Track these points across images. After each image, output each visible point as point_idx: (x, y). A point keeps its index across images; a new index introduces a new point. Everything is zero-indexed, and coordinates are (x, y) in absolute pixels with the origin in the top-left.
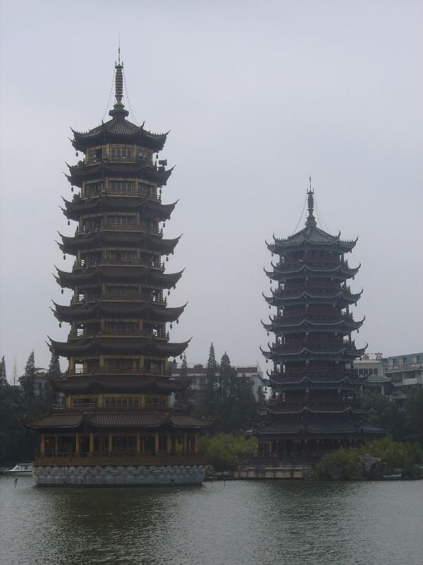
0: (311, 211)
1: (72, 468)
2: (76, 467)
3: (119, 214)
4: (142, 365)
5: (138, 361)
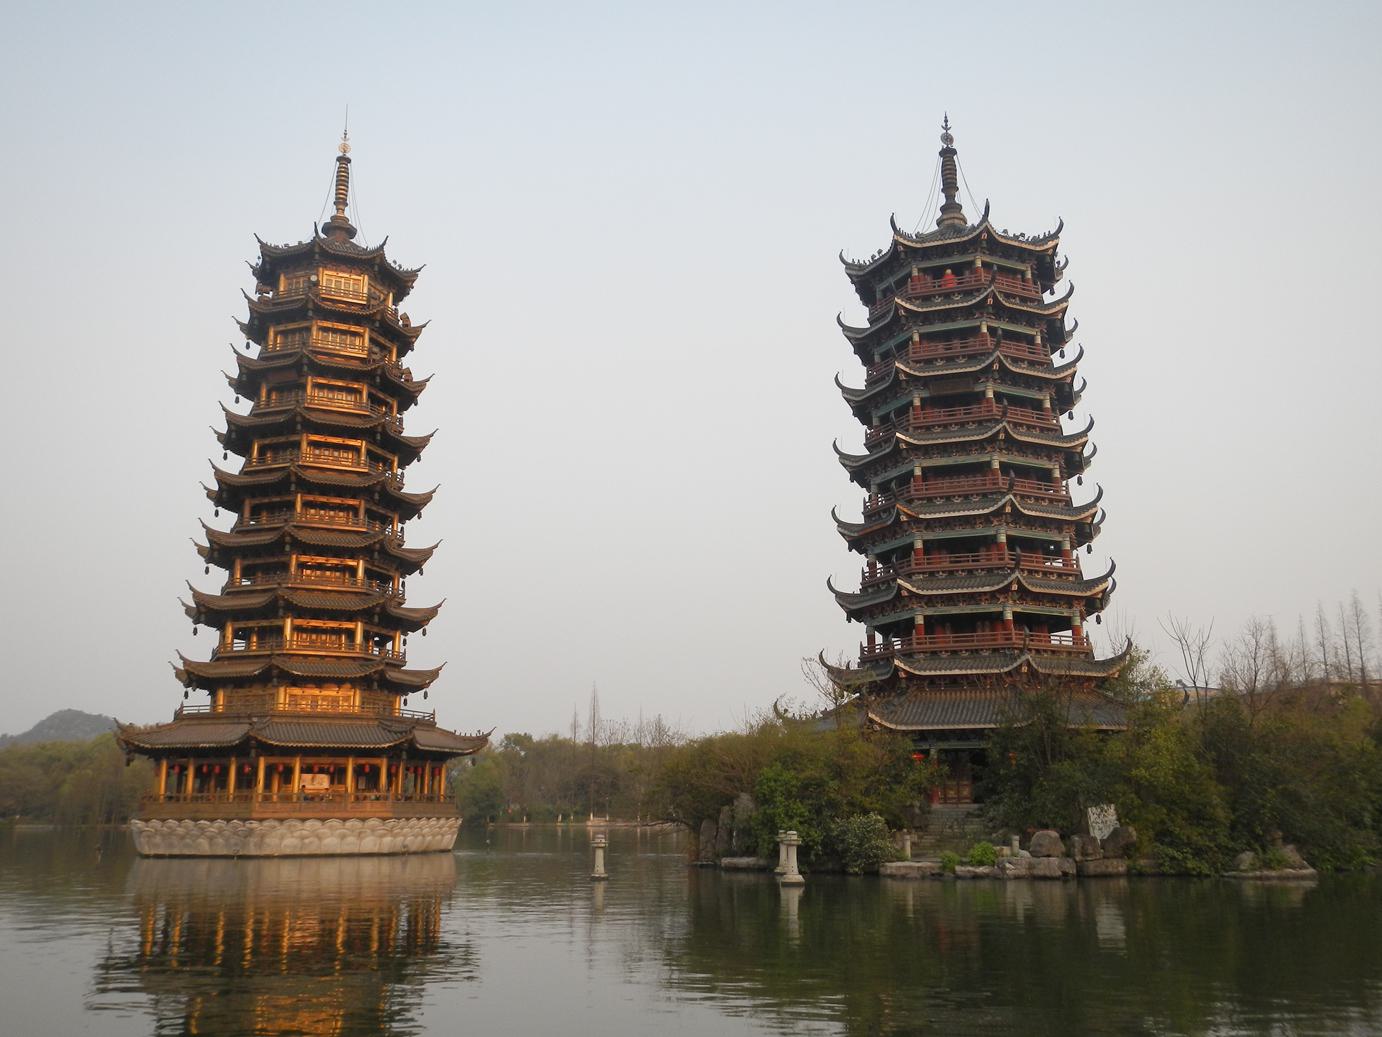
4: (359, 638)
5: (351, 634)
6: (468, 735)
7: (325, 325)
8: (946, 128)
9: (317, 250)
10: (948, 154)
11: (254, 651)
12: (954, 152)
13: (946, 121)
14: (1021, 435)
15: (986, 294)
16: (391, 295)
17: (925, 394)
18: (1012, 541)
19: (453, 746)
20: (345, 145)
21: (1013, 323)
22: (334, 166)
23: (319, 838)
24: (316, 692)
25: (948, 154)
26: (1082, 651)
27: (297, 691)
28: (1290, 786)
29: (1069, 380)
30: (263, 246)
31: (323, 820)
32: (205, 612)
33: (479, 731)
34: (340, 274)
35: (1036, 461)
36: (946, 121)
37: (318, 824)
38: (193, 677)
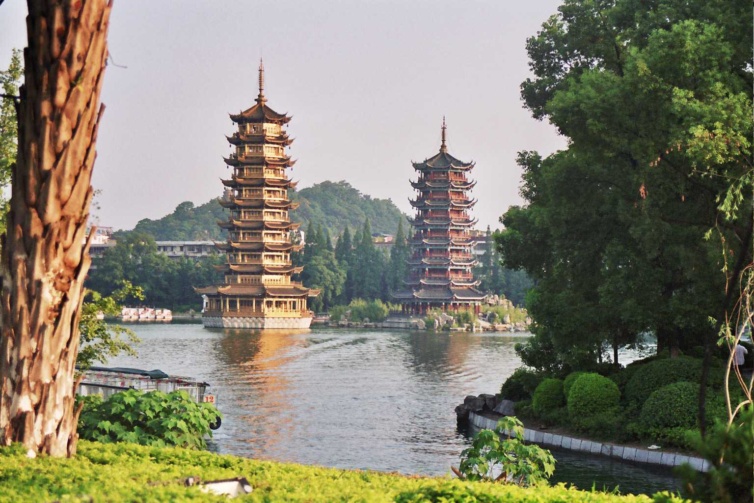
0: (443, 141)
1: (217, 318)
3: (253, 167)
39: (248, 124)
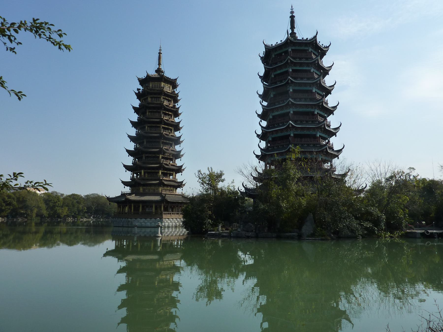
0: (293, 27)
2: (125, 218)
6: (112, 197)
7: (151, 96)
8: (292, 9)
9: (148, 78)
10: (292, 18)
11: (143, 177)
12: (294, 16)
13: (292, 7)
14: (297, 102)
15: (287, 59)
16: (171, 86)
17: (274, 93)
18: (296, 136)
19: (183, 200)
20: (160, 49)
21: (295, 66)
22: (158, 55)
23: (145, 223)
24: (149, 188)
25: (292, 18)
26: (332, 169)
27: (145, 188)
28: (46, 212)
29: (319, 82)
30: (176, 79)
31: (146, 219)
32: (179, 170)
33: (109, 196)
34: (155, 83)
35: (308, 110)
36: (292, 7)
37: (144, 220)
38: (125, 184)
39: (151, 82)
